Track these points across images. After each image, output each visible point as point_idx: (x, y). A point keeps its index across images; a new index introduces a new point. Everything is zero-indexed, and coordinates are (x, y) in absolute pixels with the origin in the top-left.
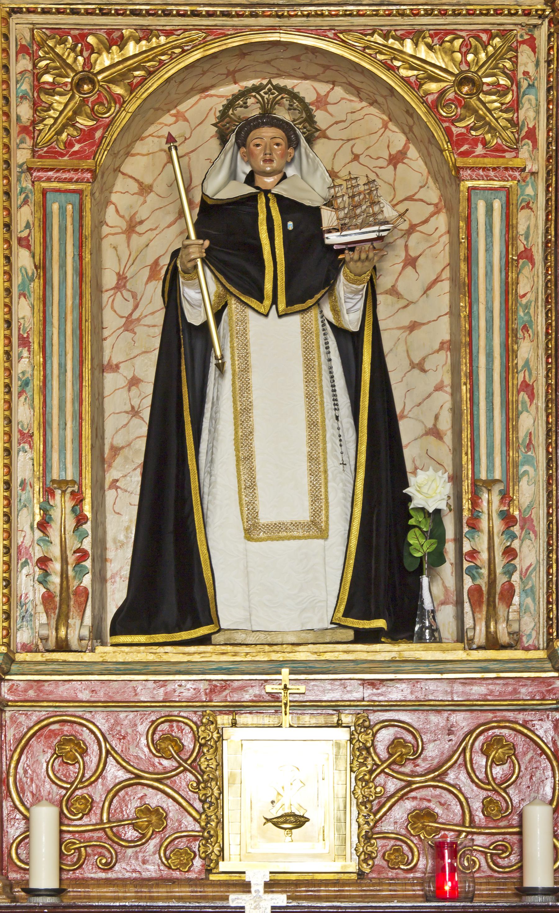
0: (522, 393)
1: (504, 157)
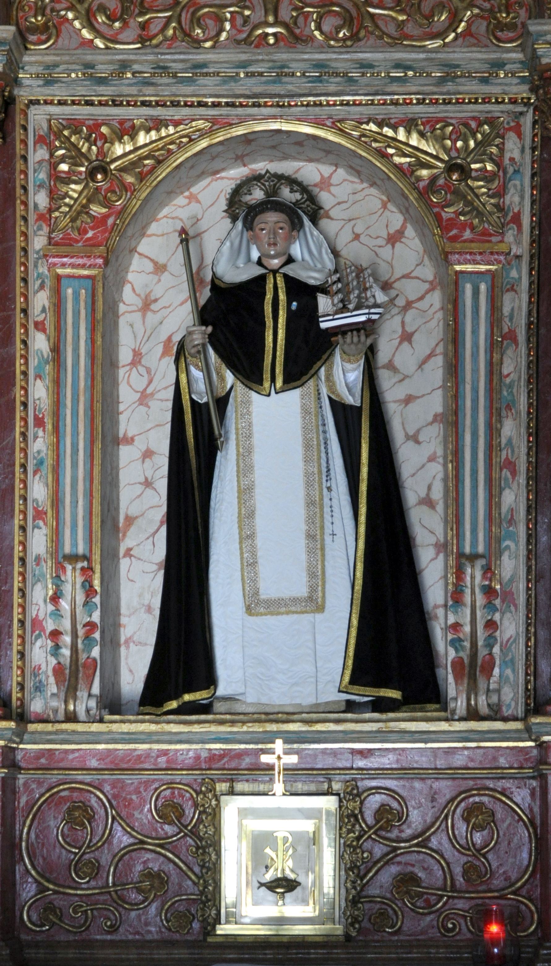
0: (505, 470)
1: (490, 241)
